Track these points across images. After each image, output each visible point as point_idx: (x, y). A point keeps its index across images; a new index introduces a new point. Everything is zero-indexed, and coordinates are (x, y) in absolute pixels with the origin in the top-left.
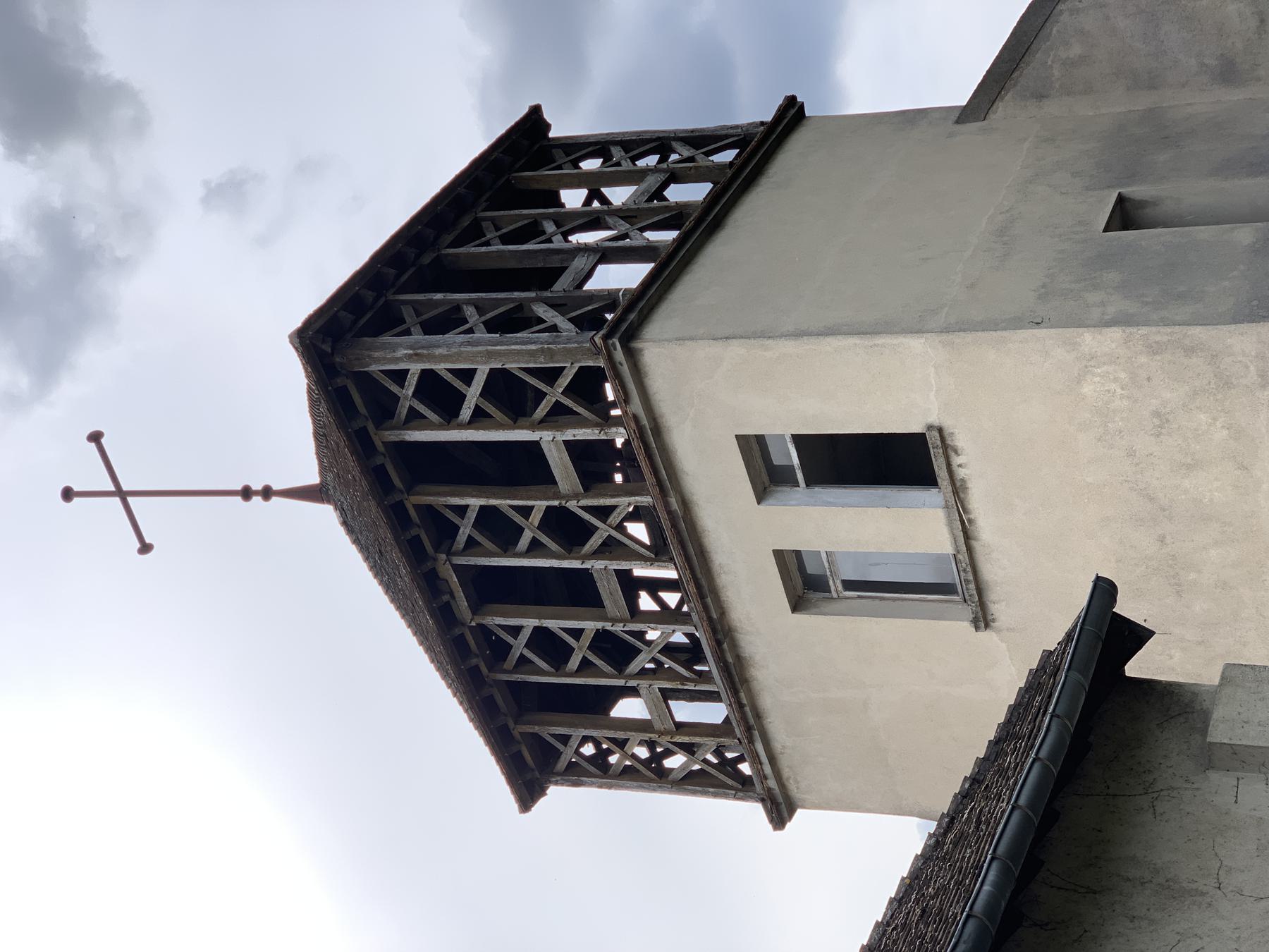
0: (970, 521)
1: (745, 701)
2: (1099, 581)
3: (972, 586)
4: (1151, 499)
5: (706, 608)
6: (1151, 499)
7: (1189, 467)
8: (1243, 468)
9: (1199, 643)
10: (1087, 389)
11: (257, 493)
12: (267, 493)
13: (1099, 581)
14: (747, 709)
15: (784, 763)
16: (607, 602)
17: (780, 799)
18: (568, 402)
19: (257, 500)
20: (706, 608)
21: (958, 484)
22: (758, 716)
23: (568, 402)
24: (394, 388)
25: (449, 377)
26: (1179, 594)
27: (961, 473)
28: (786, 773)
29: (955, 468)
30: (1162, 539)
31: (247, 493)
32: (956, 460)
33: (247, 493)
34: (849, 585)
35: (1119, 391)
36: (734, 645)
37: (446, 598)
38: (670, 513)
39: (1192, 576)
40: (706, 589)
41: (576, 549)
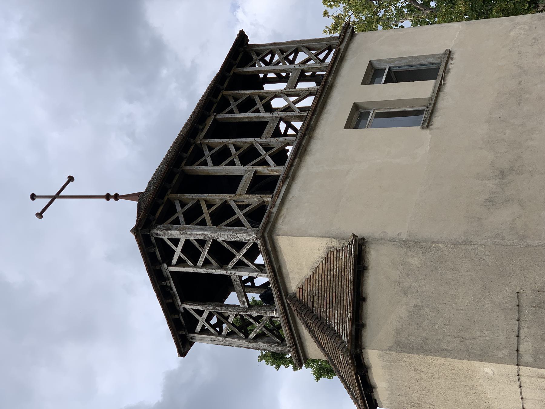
0: (444, 84)
1: (295, 164)
3: (431, 106)
4: (521, 68)
5: (311, 119)
6: (521, 68)
9: (520, 126)
10: (512, 34)
11: (112, 197)
14: (293, 168)
16: (248, 196)
17: (272, 220)
19: (112, 194)
20: (311, 119)
21: (447, 70)
22: (293, 179)
25: (193, 312)
27: (450, 66)
28: (284, 212)
29: (449, 63)
31: (108, 197)
32: (451, 62)
33: (108, 197)
34: (378, 115)
35: (523, 33)
37: (201, 127)
39: (528, 96)
40: (317, 112)
41: (224, 266)
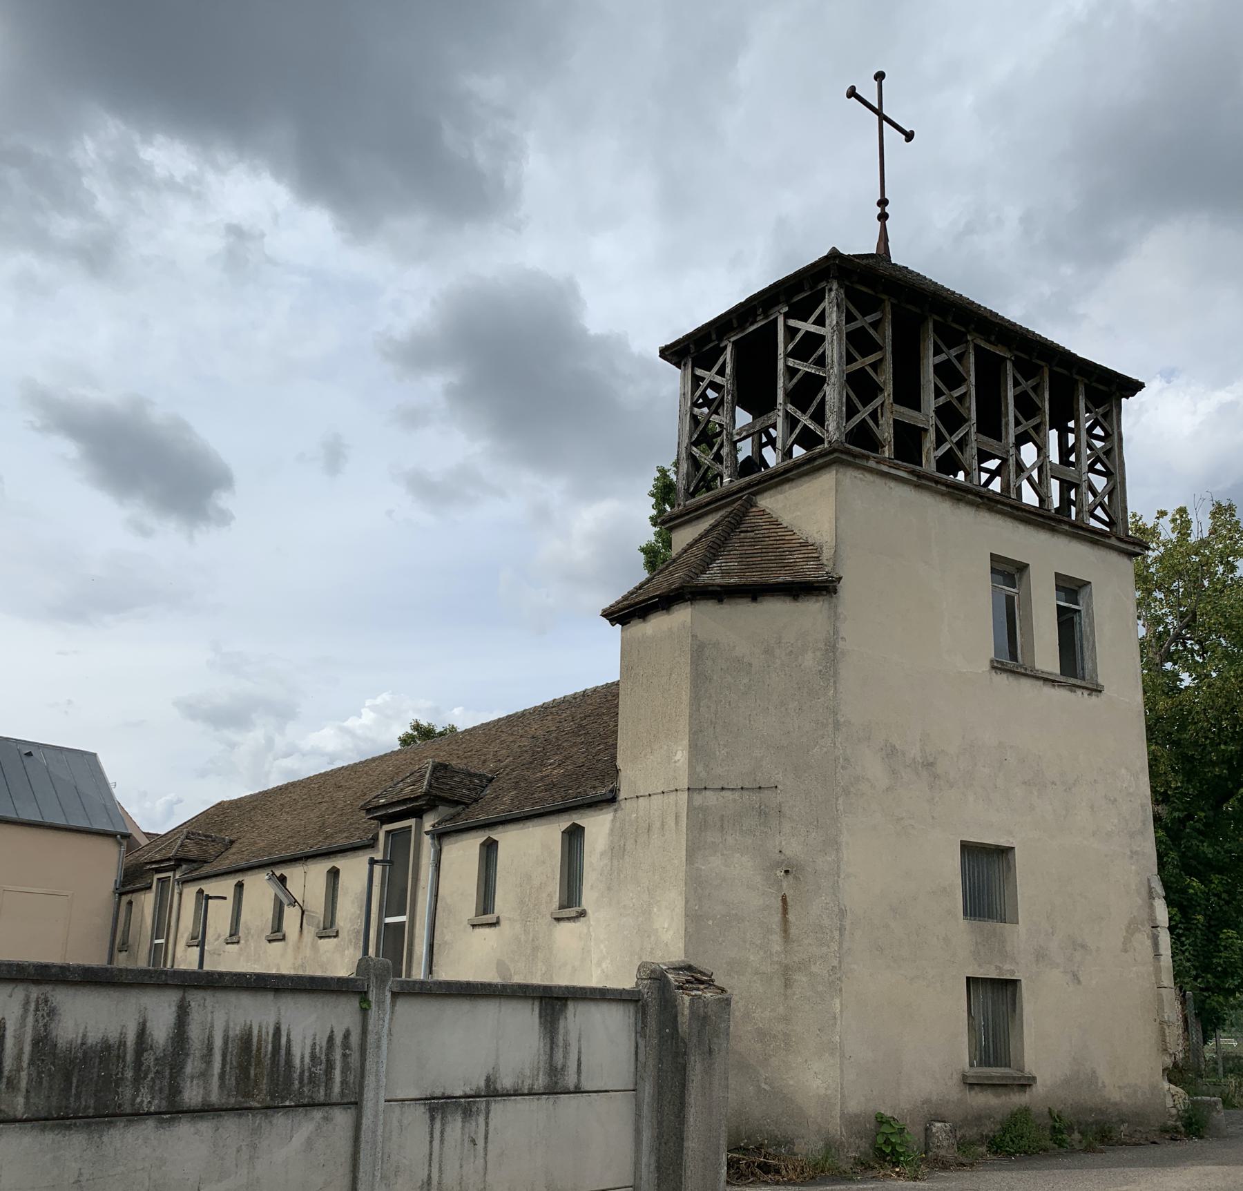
2: (219, 479)
7: (1092, 807)
8: (1094, 834)
10: (1123, 771)
12: (883, 217)
13: (219, 479)
15: (879, 481)
17: (858, 461)
18: (812, 409)
19: (887, 209)
23: (812, 409)
24: (813, 318)
26: (1024, 783)
27: (1079, 692)
30: (1054, 783)
32: (1086, 693)
33: (883, 202)
34: (1010, 600)
36: (971, 503)
38: (867, 458)
